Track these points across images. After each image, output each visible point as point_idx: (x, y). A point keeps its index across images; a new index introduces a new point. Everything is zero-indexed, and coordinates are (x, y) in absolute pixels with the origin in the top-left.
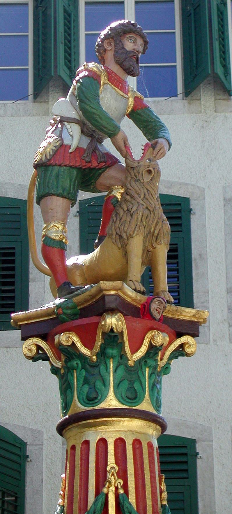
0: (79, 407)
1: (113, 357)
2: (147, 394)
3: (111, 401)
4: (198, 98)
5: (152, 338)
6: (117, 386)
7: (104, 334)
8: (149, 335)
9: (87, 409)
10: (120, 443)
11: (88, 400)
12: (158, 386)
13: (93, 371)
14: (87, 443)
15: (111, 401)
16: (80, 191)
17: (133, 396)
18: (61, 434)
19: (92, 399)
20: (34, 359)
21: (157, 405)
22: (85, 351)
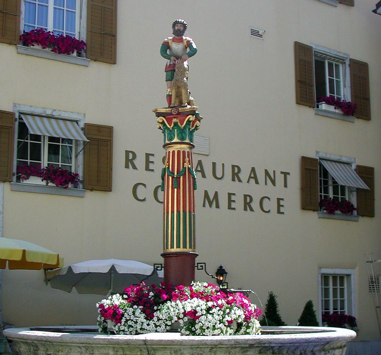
0: (167, 142)
1: (175, 129)
2: (187, 136)
3: (176, 140)
4: (19, 182)
5: (190, 118)
6: (178, 136)
7: (174, 123)
8: (189, 116)
9: (169, 142)
10: (179, 152)
11: (170, 139)
12: (187, 87)
13: (171, 132)
14: (169, 152)
15: (176, 140)
16: (150, 156)
17: (183, 138)
18: (164, 148)
19: (171, 139)
20: (159, 128)
21: (191, 140)
22: (169, 127)
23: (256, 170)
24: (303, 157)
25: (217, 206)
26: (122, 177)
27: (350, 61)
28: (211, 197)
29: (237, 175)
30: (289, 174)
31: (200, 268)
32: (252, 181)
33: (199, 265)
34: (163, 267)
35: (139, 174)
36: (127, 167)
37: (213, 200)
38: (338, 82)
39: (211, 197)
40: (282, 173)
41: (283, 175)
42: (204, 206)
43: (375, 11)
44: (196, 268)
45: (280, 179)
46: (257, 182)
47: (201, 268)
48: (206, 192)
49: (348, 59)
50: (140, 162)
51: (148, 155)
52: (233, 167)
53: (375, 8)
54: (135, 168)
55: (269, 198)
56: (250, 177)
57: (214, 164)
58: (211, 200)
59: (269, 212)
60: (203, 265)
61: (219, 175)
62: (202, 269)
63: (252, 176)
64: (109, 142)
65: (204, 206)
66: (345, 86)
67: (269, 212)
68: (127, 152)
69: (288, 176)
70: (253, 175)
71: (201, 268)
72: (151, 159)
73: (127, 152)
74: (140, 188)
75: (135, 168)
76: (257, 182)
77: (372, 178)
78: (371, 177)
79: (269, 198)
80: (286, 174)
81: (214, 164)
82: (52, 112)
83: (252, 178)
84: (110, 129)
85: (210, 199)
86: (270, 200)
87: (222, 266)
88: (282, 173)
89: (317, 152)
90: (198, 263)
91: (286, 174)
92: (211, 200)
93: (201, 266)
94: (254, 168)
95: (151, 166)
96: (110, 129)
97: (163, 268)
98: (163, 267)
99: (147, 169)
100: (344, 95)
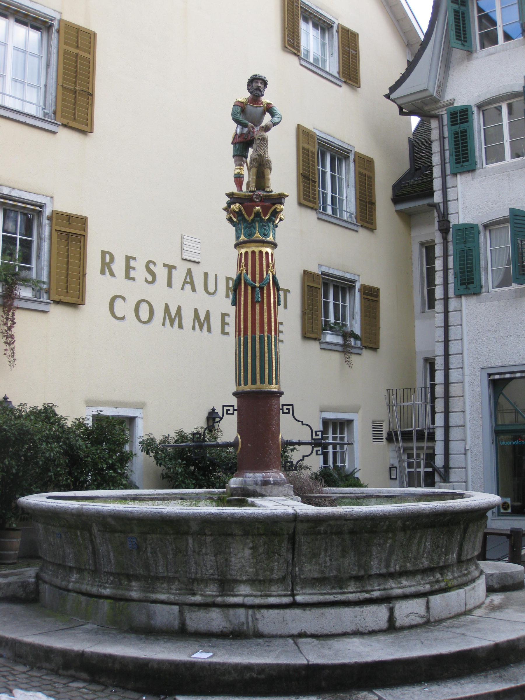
23: (193, 272)
24: (305, 271)
25: (209, 330)
26: (98, 286)
27: (355, 155)
28: (202, 317)
29: (109, 265)
30: (175, 267)
31: (285, 411)
32: (188, 287)
33: (285, 407)
34: (236, 410)
35: (117, 284)
36: (103, 272)
37: (204, 321)
38: (341, 180)
39: (202, 317)
40: (165, 265)
41: (166, 270)
42: (194, 328)
43: (388, 96)
44: (236, 408)
45: (161, 273)
46: (194, 290)
47: (287, 411)
48: (196, 311)
49: (353, 152)
50: (119, 266)
51: (128, 259)
52: (104, 253)
53: (387, 92)
54: (112, 274)
55: (124, 299)
56: (185, 282)
57: (206, 275)
58: (173, 317)
59: (123, 318)
60: (290, 407)
61: (211, 289)
62: (289, 413)
63: (188, 280)
64: (82, 238)
65: (194, 328)
66: (348, 186)
67: (123, 318)
68: (104, 253)
69: (174, 271)
70: (189, 280)
71: (287, 411)
72: (132, 263)
73: (104, 253)
74: (118, 303)
75: (112, 274)
76: (194, 290)
77: (84, 236)
78: (375, 299)
79: (124, 299)
80: (170, 268)
81: (206, 275)
82: (10, 192)
83: (188, 283)
84: (83, 221)
85: (171, 315)
86: (125, 301)
87: (7, 396)
88: (165, 265)
89: (320, 265)
90: (283, 405)
91: (170, 268)
92: (173, 317)
93: (287, 409)
94: (190, 269)
95: (132, 274)
96: (83, 221)
97: (236, 412)
98: (236, 410)
99: (128, 276)
100: (347, 197)
